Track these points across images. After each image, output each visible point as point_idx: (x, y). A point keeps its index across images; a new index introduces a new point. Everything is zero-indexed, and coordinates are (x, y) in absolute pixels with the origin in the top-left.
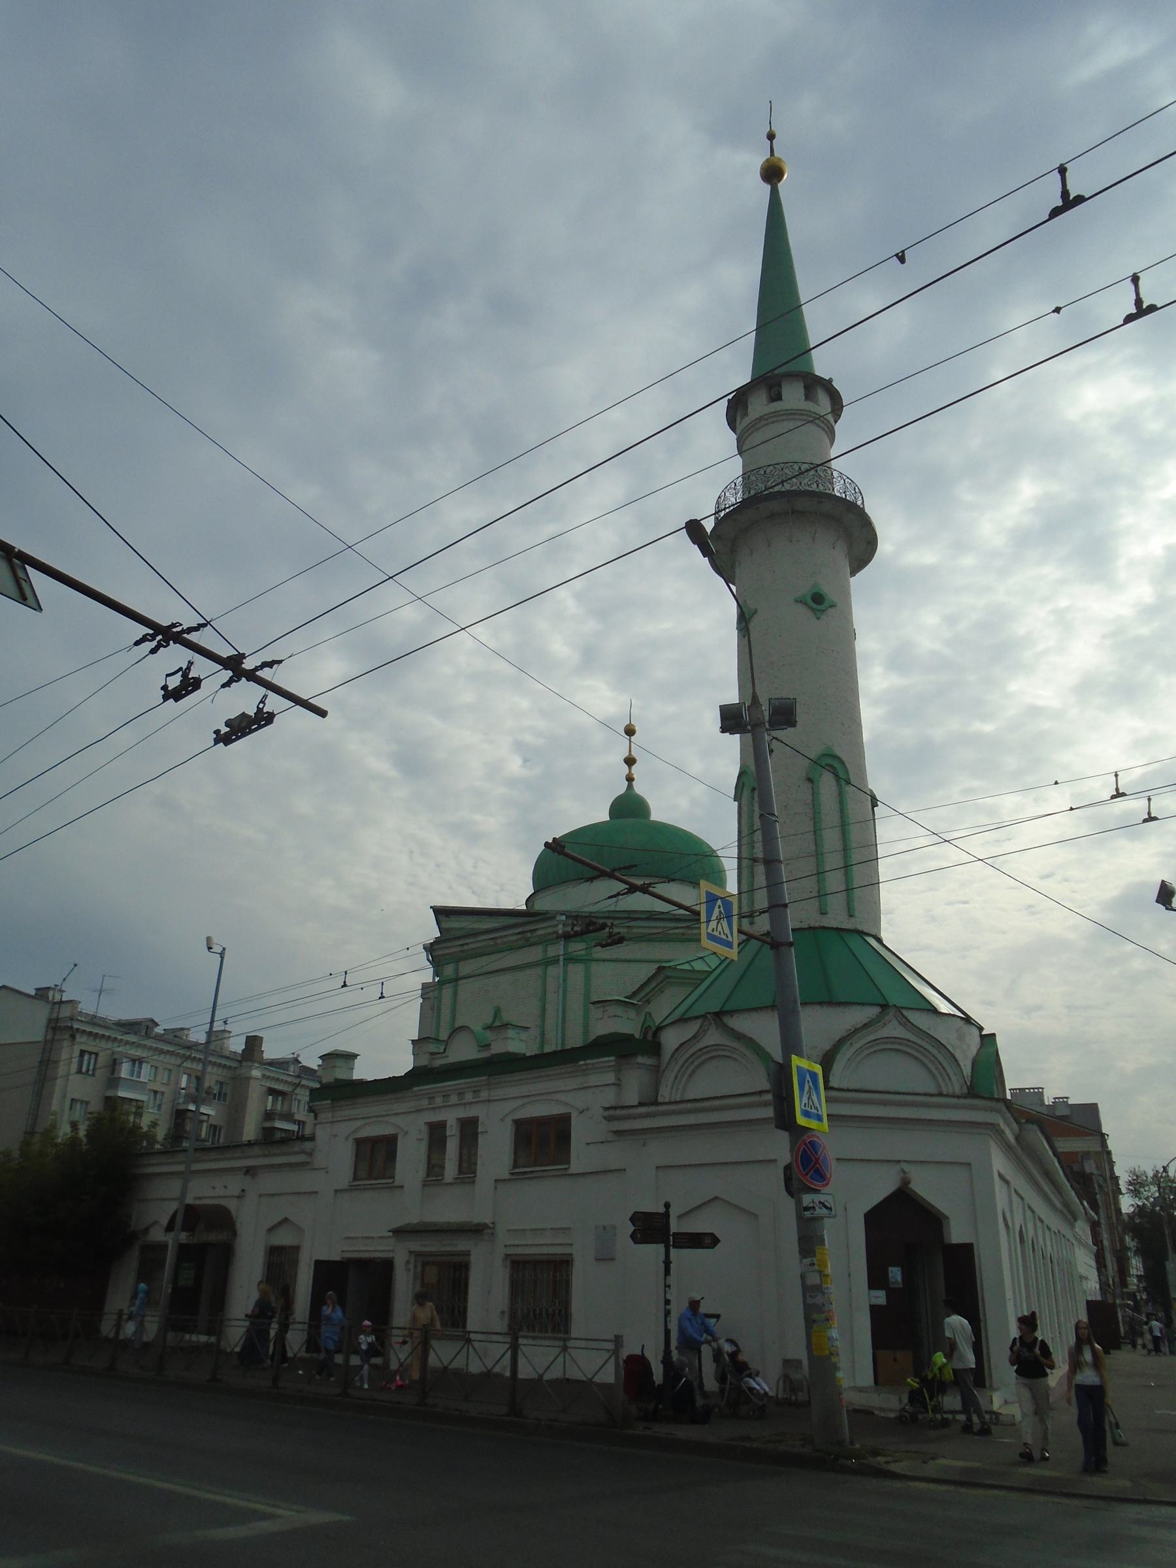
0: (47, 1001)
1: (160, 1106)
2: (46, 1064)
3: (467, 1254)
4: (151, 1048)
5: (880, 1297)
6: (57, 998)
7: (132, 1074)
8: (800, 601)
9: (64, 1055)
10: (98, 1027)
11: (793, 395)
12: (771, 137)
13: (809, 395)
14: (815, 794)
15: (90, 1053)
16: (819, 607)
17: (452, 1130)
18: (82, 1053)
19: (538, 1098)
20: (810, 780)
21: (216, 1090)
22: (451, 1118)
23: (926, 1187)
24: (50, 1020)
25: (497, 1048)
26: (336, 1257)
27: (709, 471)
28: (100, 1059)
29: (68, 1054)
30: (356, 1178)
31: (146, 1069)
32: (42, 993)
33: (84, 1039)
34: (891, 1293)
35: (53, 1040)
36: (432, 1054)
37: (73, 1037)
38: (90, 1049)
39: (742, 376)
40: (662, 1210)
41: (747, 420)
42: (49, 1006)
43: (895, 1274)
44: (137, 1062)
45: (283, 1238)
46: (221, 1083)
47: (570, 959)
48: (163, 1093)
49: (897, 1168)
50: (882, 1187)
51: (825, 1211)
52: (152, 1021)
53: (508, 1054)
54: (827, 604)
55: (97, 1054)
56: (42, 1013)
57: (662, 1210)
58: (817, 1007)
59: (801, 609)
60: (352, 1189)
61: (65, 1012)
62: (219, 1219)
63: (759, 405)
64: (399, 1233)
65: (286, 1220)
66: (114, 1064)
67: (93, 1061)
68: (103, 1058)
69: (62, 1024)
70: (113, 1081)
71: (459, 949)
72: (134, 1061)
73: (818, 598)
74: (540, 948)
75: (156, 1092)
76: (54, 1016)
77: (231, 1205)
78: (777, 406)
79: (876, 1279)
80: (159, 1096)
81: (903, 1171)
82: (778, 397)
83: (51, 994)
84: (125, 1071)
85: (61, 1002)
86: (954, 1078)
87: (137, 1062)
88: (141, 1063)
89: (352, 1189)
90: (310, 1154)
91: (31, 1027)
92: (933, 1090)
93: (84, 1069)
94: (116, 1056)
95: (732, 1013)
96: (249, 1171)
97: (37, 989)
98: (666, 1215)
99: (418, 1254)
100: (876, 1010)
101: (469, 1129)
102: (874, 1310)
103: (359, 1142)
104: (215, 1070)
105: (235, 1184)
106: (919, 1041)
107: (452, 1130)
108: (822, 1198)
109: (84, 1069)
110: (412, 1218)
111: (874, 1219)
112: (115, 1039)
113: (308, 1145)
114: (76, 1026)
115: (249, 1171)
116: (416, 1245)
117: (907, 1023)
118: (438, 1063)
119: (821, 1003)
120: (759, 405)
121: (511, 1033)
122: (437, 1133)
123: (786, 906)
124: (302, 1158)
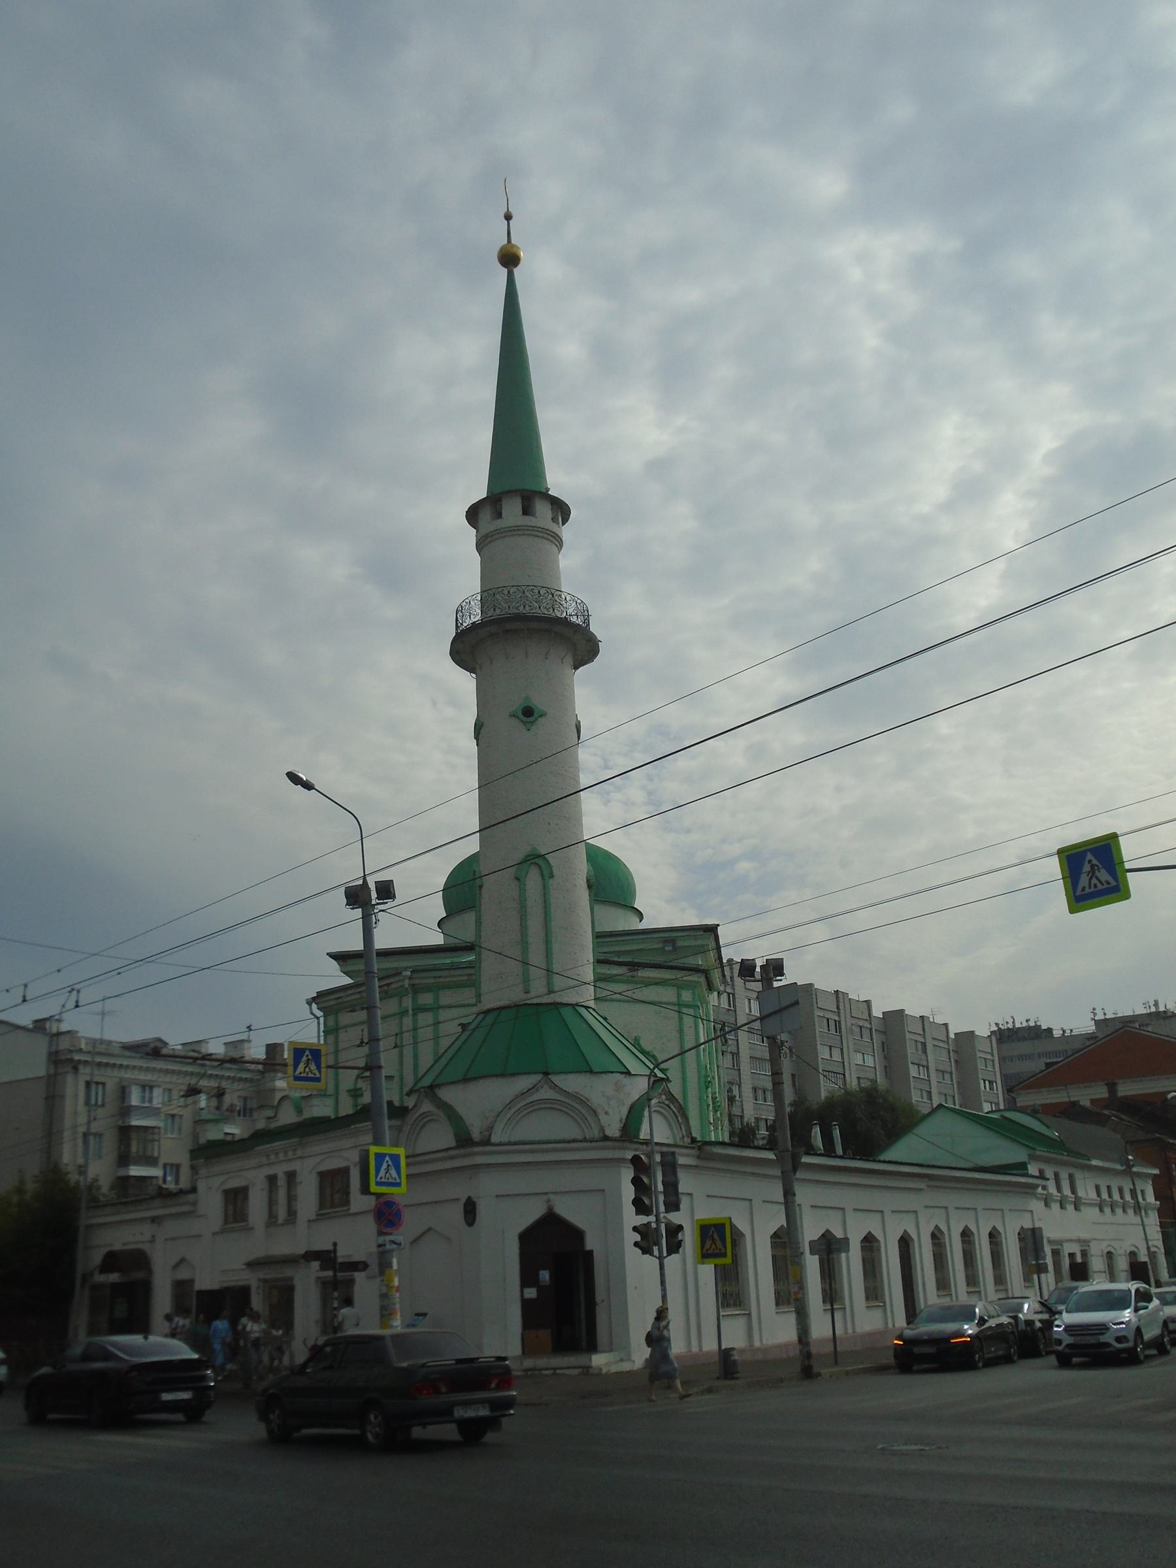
0: (45, 1034)
1: (180, 1129)
2: (53, 1098)
3: (291, 1279)
4: (160, 1070)
5: (531, 1293)
6: (54, 1030)
7: (143, 1099)
8: (513, 715)
9: (69, 1091)
10: (103, 1055)
11: (512, 510)
12: (508, 217)
13: (527, 511)
14: (522, 891)
15: (97, 1083)
16: (531, 719)
17: (282, 1182)
18: (88, 1084)
19: (339, 1153)
20: (518, 879)
21: (239, 1105)
22: (280, 1170)
23: (569, 1211)
24: (50, 1054)
25: (307, 1115)
26: (216, 1286)
27: (459, 577)
28: (108, 1086)
29: (73, 1088)
30: (226, 1222)
31: (157, 1092)
32: (40, 1025)
33: (88, 1070)
34: (541, 1289)
35: (56, 1075)
36: (269, 1118)
37: (76, 1069)
38: (96, 1079)
39: (480, 492)
40: (331, 1248)
41: (499, 524)
42: (47, 1039)
43: (545, 1276)
44: (147, 1087)
45: (183, 1274)
46: (245, 1099)
47: (418, 1010)
48: (181, 1116)
49: (545, 1197)
50: (532, 1213)
51: (395, 1246)
52: (160, 1040)
53: (313, 1118)
54: (536, 715)
55: (104, 1084)
56: (40, 1048)
57: (331, 1248)
58: (494, 1079)
59: (514, 721)
60: (223, 1231)
61: (64, 1044)
62: (137, 1260)
63: (485, 516)
64: (252, 1265)
65: (430, 1229)
66: (123, 1092)
67: (100, 1093)
68: (111, 1085)
69: (63, 1057)
70: (125, 1111)
71: (335, 1002)
72: (143, 1087)
73: (528, 712)
74: (395, 1000)
75: (173, 1116)
76: (54, 1049)
77: (146, 1247)
78: (499, 524)
79: (528, 1278)
80: (177, 1118)
81: (548, 1201)
82: (499, 515)
83: (48, 1025)
84: (135, 1099)
85: (59, 1034)
86: (593, 1125)
87: (147, 1087)
88: (151, 1088)
89: (223, 1231)
90: (195, 1204)
91: (32, 1063)
92: (580, 1137)
93: (93, 1102)
94: (124, 1084)
95: (439, 1086)
96: (154, 1220)
97: (36, 1022)
98: (335, 1251)
99: (265, 1281)
100: (540, 1077)
101: (291, 1176)
102: (526, 1304)
103: (227, 1192)
104: (236, 1086)
105: (147, 1231)
106: (567, 1100)
107: (282, 1182)
108: (392, 1238)
109: (93, 1102)
110: (260, 1253)
111: (526, 1237)
112: (121, 1065)
113: (191, 1197)
114: (77, 1057)
115: (154, 1220)
116: (262, 1274)
117: (555, 1087)
118: (273, 1125)
119: (497, 1076)
120: (485, 516)
121: (315, 1101)
122: (272, 1179)
123: (378, 1040)
124: (185, 1208)
